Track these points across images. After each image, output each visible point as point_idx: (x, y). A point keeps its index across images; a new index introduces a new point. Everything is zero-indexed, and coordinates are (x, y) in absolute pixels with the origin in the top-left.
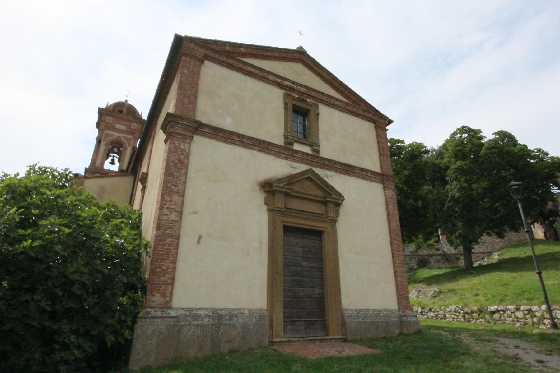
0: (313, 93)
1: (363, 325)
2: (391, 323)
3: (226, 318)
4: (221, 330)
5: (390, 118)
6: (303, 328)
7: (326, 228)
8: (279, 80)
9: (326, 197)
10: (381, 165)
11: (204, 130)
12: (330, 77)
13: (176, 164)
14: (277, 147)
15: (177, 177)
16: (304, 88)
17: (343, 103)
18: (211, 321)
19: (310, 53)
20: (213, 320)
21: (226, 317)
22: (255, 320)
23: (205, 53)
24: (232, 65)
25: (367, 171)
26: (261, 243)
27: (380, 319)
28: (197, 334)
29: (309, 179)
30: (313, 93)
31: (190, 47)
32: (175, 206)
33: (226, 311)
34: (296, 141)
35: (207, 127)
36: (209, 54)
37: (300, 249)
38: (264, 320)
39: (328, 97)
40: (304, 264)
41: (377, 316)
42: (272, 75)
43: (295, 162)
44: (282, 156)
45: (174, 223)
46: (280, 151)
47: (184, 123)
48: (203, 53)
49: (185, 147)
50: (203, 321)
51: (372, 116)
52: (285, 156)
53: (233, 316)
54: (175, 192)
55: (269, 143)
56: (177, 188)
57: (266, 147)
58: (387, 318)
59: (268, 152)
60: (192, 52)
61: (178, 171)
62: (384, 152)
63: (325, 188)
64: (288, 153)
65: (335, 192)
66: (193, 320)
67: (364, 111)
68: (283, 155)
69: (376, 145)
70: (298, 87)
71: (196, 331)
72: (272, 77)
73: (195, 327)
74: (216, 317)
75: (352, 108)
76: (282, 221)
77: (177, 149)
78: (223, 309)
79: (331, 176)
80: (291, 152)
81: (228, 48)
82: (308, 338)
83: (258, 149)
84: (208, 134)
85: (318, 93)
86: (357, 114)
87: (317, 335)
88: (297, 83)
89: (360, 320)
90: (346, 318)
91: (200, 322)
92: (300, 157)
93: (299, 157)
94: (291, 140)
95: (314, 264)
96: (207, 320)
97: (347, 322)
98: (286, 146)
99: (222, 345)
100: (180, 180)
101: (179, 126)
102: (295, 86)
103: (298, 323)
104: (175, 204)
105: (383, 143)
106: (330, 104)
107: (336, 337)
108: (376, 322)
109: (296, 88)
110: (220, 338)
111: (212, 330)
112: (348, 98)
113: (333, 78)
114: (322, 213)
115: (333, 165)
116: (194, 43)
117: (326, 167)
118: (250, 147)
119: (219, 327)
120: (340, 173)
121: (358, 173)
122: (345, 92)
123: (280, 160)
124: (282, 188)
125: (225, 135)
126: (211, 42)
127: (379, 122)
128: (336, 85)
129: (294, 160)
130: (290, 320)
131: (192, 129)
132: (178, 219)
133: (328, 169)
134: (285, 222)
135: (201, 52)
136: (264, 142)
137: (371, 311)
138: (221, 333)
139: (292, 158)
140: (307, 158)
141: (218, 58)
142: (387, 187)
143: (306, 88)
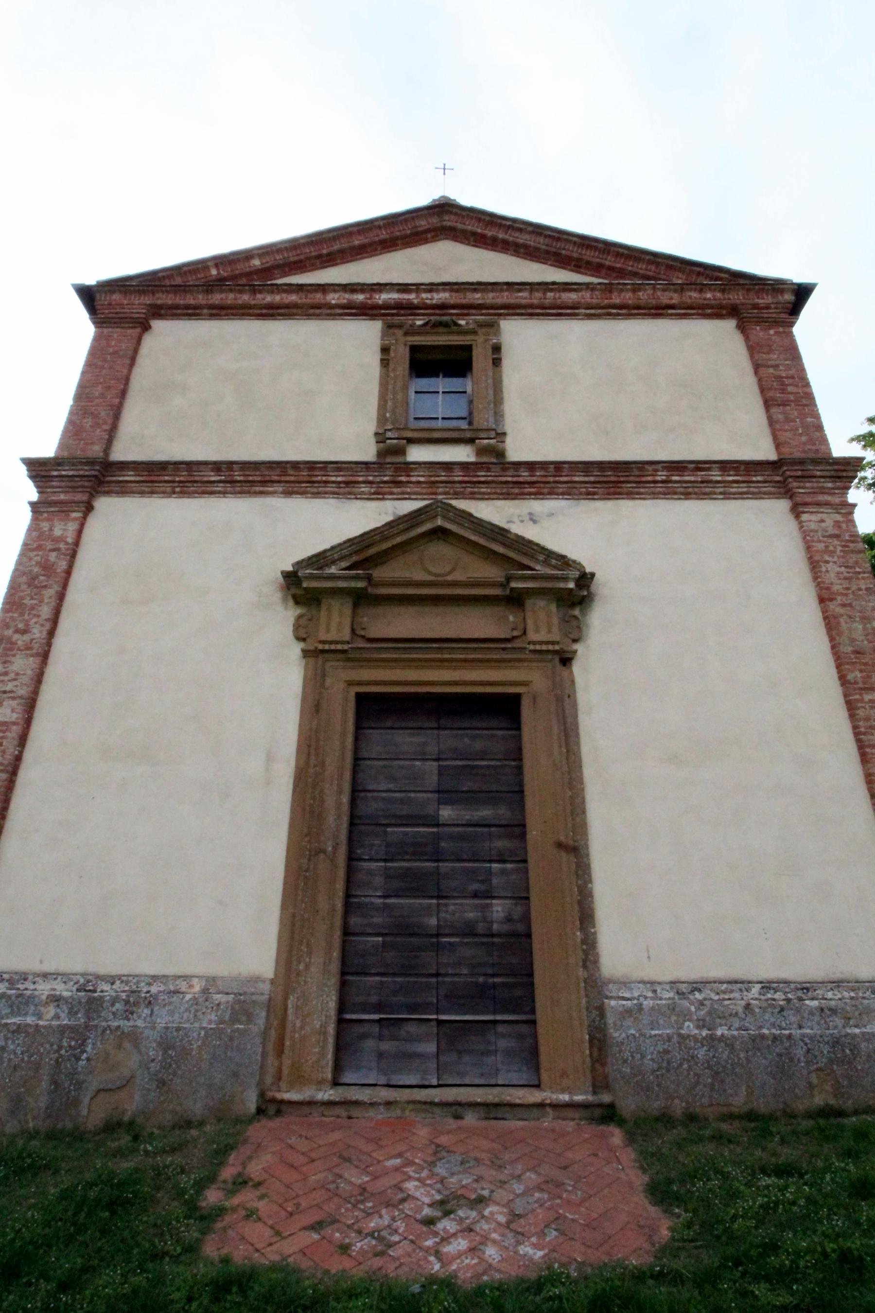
0: (477, 297)
1: (701, 1053)
2: (863, 1045)
3: (114, 1009)
4: (89, 1049)
5: (798, 278)
6: (430, 1047)
7: (525, 684)
8: (360, 297)
9: (509, 579)
10: (775, 438)
11: (121, 479)
12: (541, 240)
13: (35, 578)
14: (339, 469)
15: (32, 608)
16: (444, 290)
17: (593, 290)
18: (62, 1015)
19: (465, 200)
20: (72, 1013)
21: (113, 1005)
22: (213, 1017)
23: (148, 302)
24: (221, 307)
25: (700, 466)
26: (270, 758)
27: (800, 1027)
28: (12, 1056)
29: (440, 533)
30: (478, 295)
31: (114, 303)
32: (15, 683)
33: (127, 983)
34: (411, 441)
35: (129, 469)
36: (159, 302)
37: (432, 767)
38: (250, 1017)
39: (531, 291)
40: (446, 813)
41: (782, 1010)
42: (335, 291)
43: (409, 499)
44: (363, 493)
45: (5, 728)
46: (351, 479)
47: (64, 473)
48: (145, 304)
49: (65, 530)
50: (40, 1018)
51: (719, 295)
52: (373, 490)
53: (136, 1004)
54: (19, 649)
55: (311, 466)
56: (26, 638)
57: (305, 479)
58: (839, 1022)
59: (315, 490)
60: (121, 313)
61: (36, 594)
62: (783, 391)
63: (501, 550)
64: (378, 479)
65: (541, 557)
66: (9, 1010)
67: (682, 290)
68: (365, 489)
69: (751, 380)
70: (424, 295)
71: (12, 1047)
72: (336, 296)
73: (9, 1035)
74: (80, 1002)
75: (629, 295)
76: (350, 683)
77: (44, 540)
78: (119, 977)
79: (551, 515)
80: (388, 473)
81: (214, 272)
82: (436, 1094)
83: (281, 489)
84: (133, 485)
85: (492, 291)
86: (657, 307)
87: (493, 1082)
88: (417, 285)
89: (689, 1028)
90: (610, 1019)
91: (30, 1020)
92: (422, 479)
93: (419, 482)
94: (395, 441)
95: (485, 813)
96: (51, 1011)
97: (617, 1035)
98: (382, 461)
99: (86, 1101)
100: (39, 616)
101: (54, 484)
102: (412, 296)
103: (412, 1028)
104: (15, 680)
105: (776, 367)
106: (544, 308)
107: (565, 1097)
108: (775, 1038)
109: (415, 301)
110: (81, 1077)
111: (60, 1047)
112: (595, 269)
113: (553, 237)
114: (508, 636)
115: (551, 479)
116: (120, 292)
117: (526, 490)
118: (258, 489)
119: (84, 1043)
120: (590, 496)
121: (663, 482)
122: (602, 261)
123: (359, 503)
124: (332, 577)
125: (180, 476)
126: (169, 273)
127: (756, 306)
128: (568, 253)
129: (403, 493)
130: (376, 1017)
131: (86, 484)
132: (17, 718)
133: (539, 495)
134: (360, 683)
135: (139, 304)
136: (295, 465)
137: (756, 989)
138: (88, 1059)
139: (395, 490)
140: (451, 479)
141: (182, 302)
142: (806, 504)
143: (452, 290)
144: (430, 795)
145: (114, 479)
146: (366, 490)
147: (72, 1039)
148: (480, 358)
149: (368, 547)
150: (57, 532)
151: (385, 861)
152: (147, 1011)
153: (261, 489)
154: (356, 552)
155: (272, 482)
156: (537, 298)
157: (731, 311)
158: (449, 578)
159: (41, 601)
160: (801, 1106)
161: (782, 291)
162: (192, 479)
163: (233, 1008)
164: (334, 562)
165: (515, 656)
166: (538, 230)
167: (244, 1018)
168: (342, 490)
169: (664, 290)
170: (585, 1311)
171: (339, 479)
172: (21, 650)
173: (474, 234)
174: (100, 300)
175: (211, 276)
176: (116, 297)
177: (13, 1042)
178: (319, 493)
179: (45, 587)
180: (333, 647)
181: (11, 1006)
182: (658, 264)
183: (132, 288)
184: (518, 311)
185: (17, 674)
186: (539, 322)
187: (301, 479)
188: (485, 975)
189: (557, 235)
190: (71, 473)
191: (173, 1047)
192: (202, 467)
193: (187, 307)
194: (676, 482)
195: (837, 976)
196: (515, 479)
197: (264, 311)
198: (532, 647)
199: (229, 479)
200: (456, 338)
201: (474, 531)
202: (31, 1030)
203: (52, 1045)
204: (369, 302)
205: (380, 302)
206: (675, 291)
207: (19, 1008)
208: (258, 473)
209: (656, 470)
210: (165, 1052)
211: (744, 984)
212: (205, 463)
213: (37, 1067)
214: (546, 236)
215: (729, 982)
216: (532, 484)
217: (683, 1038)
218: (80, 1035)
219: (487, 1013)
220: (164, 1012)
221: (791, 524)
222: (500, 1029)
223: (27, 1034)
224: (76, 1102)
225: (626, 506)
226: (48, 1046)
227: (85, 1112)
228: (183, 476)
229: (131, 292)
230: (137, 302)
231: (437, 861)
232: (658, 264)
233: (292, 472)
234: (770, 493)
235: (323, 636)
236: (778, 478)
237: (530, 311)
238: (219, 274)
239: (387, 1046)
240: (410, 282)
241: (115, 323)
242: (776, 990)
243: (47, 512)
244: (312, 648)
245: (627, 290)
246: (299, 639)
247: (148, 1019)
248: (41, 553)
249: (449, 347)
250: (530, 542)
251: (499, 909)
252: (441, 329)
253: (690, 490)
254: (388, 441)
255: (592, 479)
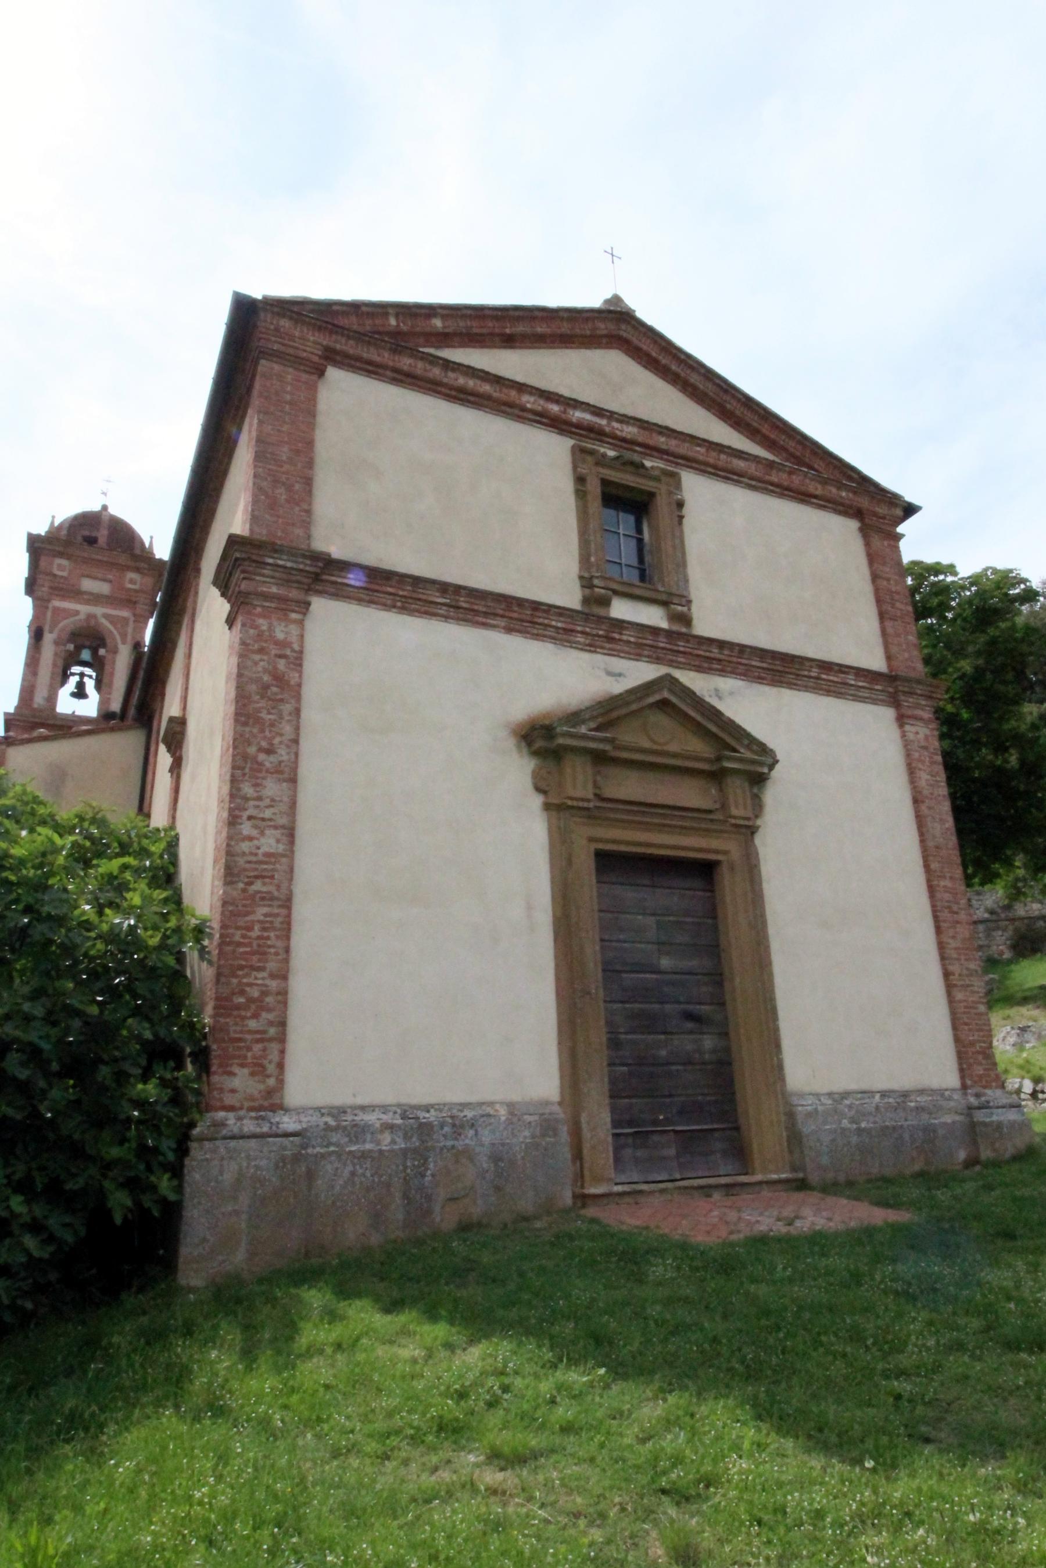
0: (661, 441)
3: (444, 1132)
4: (431, 1166)
5: (909, 497)
6: (672, 1152)
7: (726, 853)
8: (555, 408)
9: (719, 759)
12: (710, 385)
14: (561, 615)
16: (633, 425)
18: (398, 1140)
20: (406, 1137)
21: (442, 1128)
23: (325, 343)
26: (529, 907)
27: (906, 1120)
29: (664, 705)
30: (663, 439)
32: (272, 810)
33: (441, 1111)
36: (338, 347)
40: (665, 963)
42: (531, 394)
45: (273, 860)
46: (571, 627)
47: (281, 562)
50: (378, 1143)
51: (851, 495)
52: (587, 642)
53: (462, 1126)
54: (267, 771)
56: (272, 758)
59: (535, 631)
61: (273, 708)
63: (714, 729)
64: (594, 632)
66: (346, 1139)
67: (826, 483)
68: (580, 639)
69: (868, 588)
70: (615, 425)
71: (361, 1171)
72: (532, 399)
73: (356, 1161)
74: (412, 1128)
75: (785, 476)
76: (591, 840)
78: (432, 1106)
79: (731, 693)
80: (604, 627)
81: (393, 322)
83: (503, 624)
85: (675, 438)
88: (612, 413)
89: (845, 1123)
90: (800, 1119)
91: (368, 1146)
93: (629, 642)
99: (437, 1209)
100: (281, 735)
102: (604, 422)
103: (656, 1138)
104: (272, 806)
105: (888, 580)
107: (775, 1177)
109: (607, 429)
115: (735, 660)
118: (481, 619)
120: (760, 680)
124: (584, 737)
125: (403, 590)
127: (875, 514)
133: (723, 672)
136: (521, 602)
137: (877, 1097)
138: (433, 1175)
139: (608, 645)
140: (655, 644)
142: (909, 717)
143: (640, 427)
144: (650, 946)
145: (333, 578)
146: (582, 640)
147: (414, 1159)
148: (662, 506)
149: (611, 710)
150: (280, 635)
151: (622, 1002)
152: (471, 1132)
153: (484, 620)
154: (602, 715)
155: (496, 615)
156: (712, 458)
157: (857, 514)
158: (665, 748)
159: (281, 717)
160: (908, 1172)
161: (896, 505)
162: (415, 595)
163: (541, 1125)
164: (583, 722)
165: (695, 825)
166: (709, 375)
167: (551, 1133)
168: (560, 636)
169: (812, 480)
170: (381, 1565)
171: (559, 625)
172: (272, 773)
173: (648, 355)
174: (265, 321)
175: (389, 325)
176: (285, 323)
177: (361, 1167)
178: (537, 635)
179: (282, 700)
180: (581, 804)
181: (348, 1136)
182: (804, 446)
183: (307, 320)
184: (694, 465)
185: (273, 800)
186: (709, 481)
187: (524, 617)
188: (702, 1094)
189: (725, 387)
190: (289, 564)
191: (501, 1159)
192: (428, 586)
193: (370, 363)
194: (824, 680)
195: (920, 1087)
196: (708, 654)
197: (453, 393)
198: (733, 821)
199: (453, 603)
200: (589, 446)
201: (694, 708)
202: (376, 1155)
203: (397, 1166)
204: (563, 416)
205: (574, 420)
206: (820, 483)
207: (356, 1137)
208: (483, 603)
209: (811, 667)
210: (496, 1165)
211: (870, 1093)
212: (433, 582)
213: (388, 1185)
214: (715, 384)
215: (862, 1092)
216: (719, 660)
217: (843, 1130)
218: (421, 1155)
219: (706, 1124)
220: (486, 1132)
221: (894, 732)
222: (717, 1135)
223: (373, 1159)
224: (429, 1212)
225: (787, 696)
226: (394, 1167)
227: (438, 1219)
228: (406, 591)
229: (304, 323)
230: (312, 338)
231: (662, 1003)
232: (804, 446)
233: (516, 609)
234: (882, 701)
235: (571, 793)
236: (891, 690)
237: (702, 467)
238: (398, 325)
239: (639, 1153)
240: (606, 408)
241: (289, 361)
242: (889, 1097)
243: (263, 607)
244: (556, 801)
245: (785, 471)
246: (538, 789)
247: (474, 1139)
248: (265, 658)
249: (631, 489)
250: (739, 727)
251: (708, 1042)
252: (630, 468)
253: (832, 688)
254: (597, 590)
255: (764, 665)
